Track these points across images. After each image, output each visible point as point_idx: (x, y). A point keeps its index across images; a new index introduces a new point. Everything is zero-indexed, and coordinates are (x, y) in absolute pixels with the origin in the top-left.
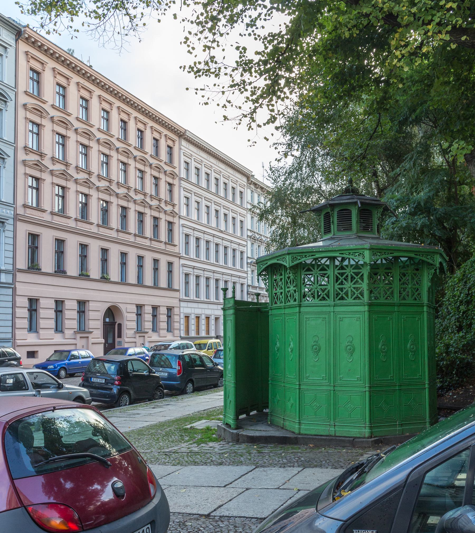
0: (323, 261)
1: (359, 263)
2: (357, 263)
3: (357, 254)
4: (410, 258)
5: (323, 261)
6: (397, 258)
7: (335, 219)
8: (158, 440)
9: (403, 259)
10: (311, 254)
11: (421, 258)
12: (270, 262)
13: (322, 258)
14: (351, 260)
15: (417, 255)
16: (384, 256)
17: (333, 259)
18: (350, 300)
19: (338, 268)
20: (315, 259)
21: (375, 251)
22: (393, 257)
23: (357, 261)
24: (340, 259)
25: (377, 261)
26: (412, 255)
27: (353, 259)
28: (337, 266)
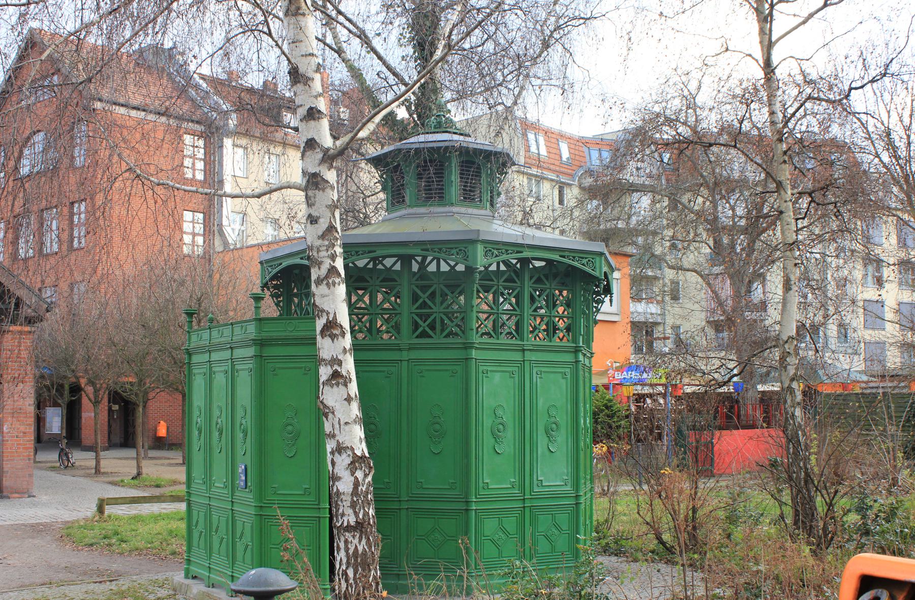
0: (388, 262)
1: (490, 269)
2: (453, 268)
3: (454, 251)
4: (549, 262)
5: (388, 262)
6: (525, 261)
7: (410, 179)
8: (778, 479)
9: (538, 264)
10: (516, 249)
11: (571, 262)
12: (285, 264)
13: (384, 257)
14: (442, 262)
15: (563, 257)
16: (504, 257)
17: (406, 260)
18: (503, 340)
19: (417, 277)
20: (374, 259)
21: (489, 246)
22: (520, 260)
23: (453, 263)
24: (419, 259)
25: (490, 265)
26: (555, 257)
27: (445, 261)
28: (415, 274)
